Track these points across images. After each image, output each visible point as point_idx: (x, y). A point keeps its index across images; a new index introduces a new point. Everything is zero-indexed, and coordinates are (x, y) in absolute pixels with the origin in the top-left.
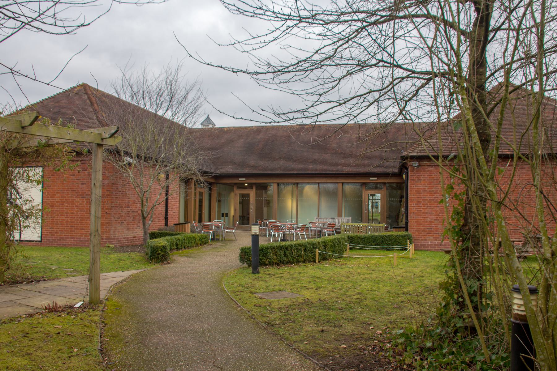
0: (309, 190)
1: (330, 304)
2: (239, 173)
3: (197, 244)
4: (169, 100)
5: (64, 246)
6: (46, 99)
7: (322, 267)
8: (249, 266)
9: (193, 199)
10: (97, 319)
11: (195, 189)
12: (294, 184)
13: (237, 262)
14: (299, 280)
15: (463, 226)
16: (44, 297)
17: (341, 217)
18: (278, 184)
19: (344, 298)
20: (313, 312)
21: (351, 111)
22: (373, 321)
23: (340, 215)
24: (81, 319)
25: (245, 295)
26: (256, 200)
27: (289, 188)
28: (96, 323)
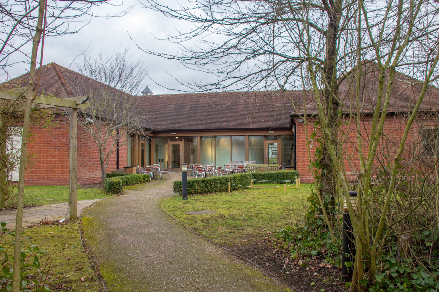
0: (224, 141)
1: (237, 217)
2: (171, 131)
3: (141, 182)
4: (119, 75)
5: (42, 184)
6: (24, 75)
7: (232, 194)
8: (181, 195)
9: (137, 148)
10: (77, 228)
11: (139, 142)
12: (213, 136)
13: (172, 193)
14: (216, 203)
15: (322, 160)
16: (37, 216)
17: (248, 160)
18: (201, 137)
19: (247, 213)
20: (225, 222)
21: (250, 83)
22: (266, 226)
23: (247, 159)
24: (66, 228)
25: (178, 213)
26: (185, 149)
27: (209, 140)
28: (77, 230)
